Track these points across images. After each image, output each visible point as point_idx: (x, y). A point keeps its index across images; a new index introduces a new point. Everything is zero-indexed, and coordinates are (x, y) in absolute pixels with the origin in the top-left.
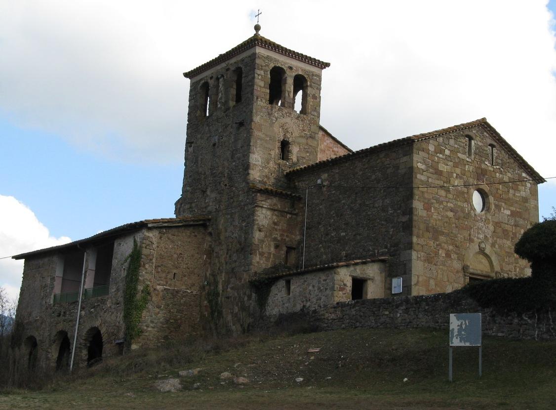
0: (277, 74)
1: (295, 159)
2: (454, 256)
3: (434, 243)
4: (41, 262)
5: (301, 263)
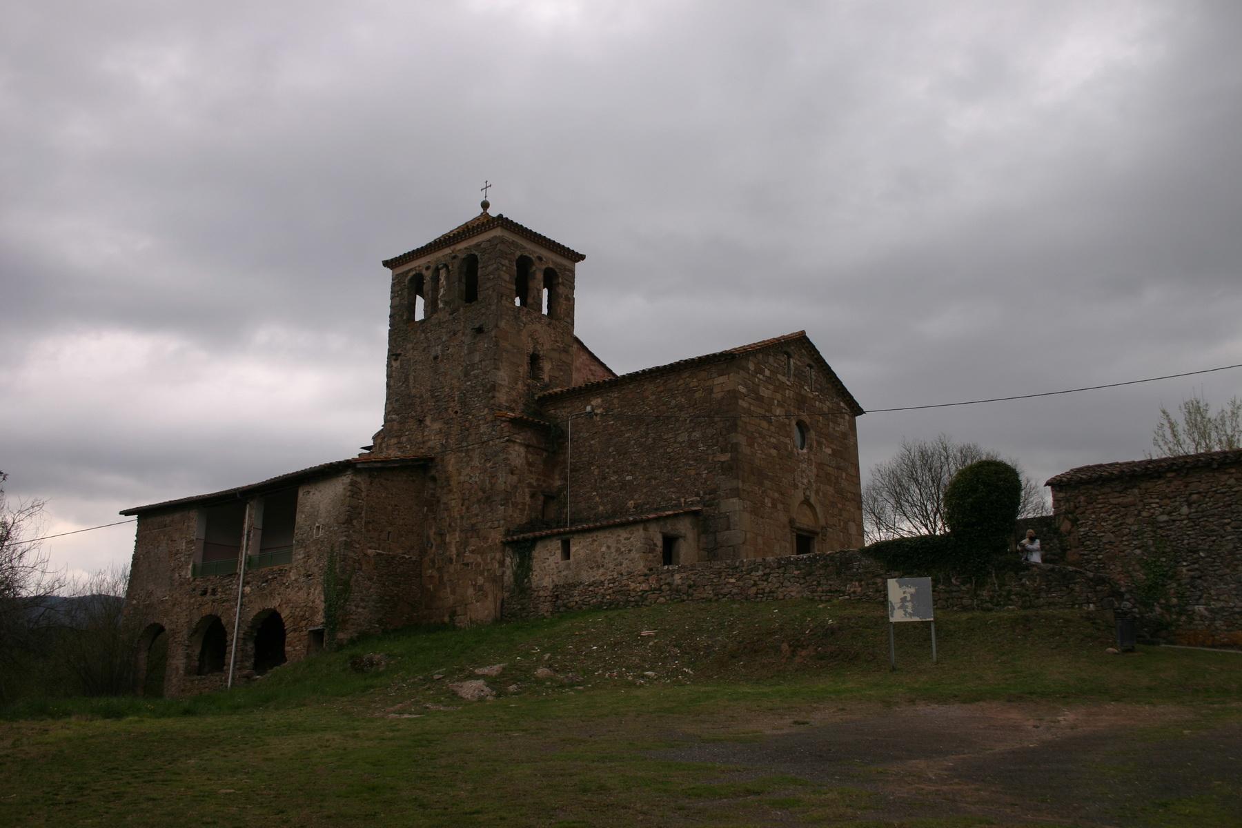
0: (524, 264)
1: (547, 379)
2: (780, 506)
3: (759, 489)
4: (167, 519)
5: (564, 516)
